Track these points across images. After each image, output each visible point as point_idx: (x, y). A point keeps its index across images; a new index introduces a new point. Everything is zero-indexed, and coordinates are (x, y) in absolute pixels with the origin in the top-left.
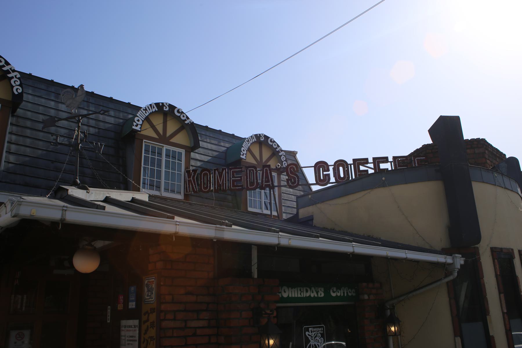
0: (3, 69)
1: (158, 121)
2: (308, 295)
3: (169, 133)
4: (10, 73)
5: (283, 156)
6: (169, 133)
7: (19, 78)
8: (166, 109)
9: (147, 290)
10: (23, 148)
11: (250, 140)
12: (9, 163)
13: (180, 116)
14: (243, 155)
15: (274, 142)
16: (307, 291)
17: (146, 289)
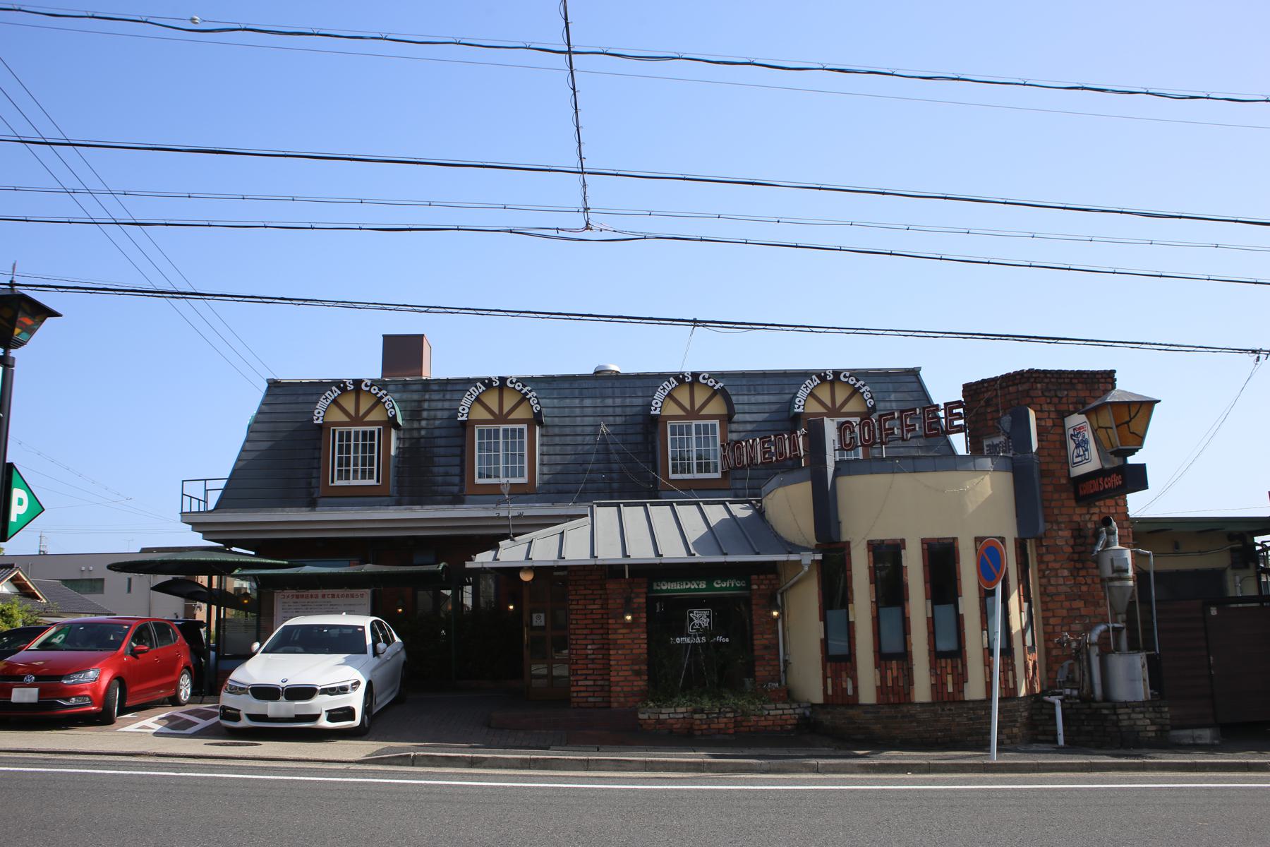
0: (856, 386)
2: (687, 587)
3: (839, 402)
6: (839, 402)
7: (869, 391)
9: (1075, 445)
10: (553, 457)
11: (473, 393)
12: (543, 474)
13: (848, 382)
16: (687, 584)
17: (1071, 445)
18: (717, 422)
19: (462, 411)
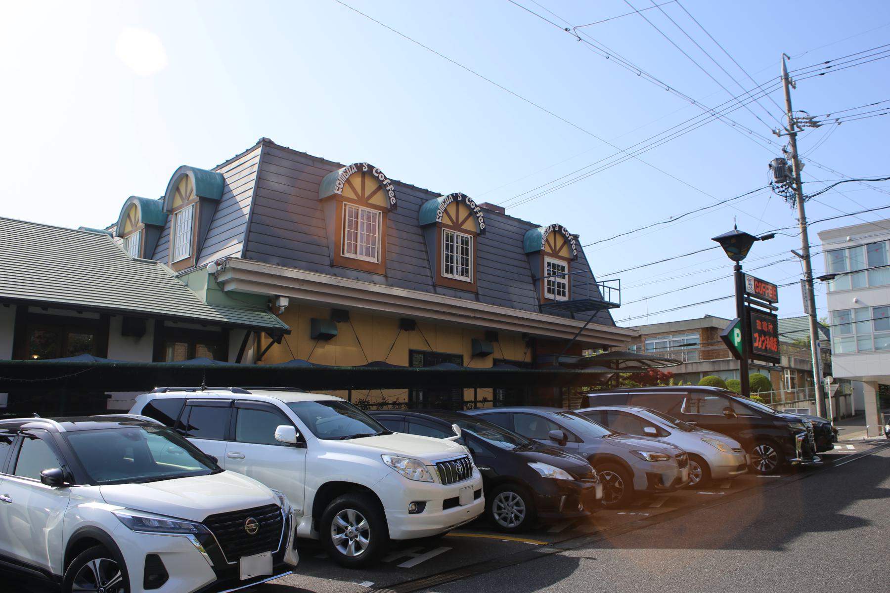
1: (357, 182)
4: (478, 213)
5: (391, 192)
7: (393, 191)
8: (365, 169)
11: (348, 171)
14: (439, 218)
15: (472, 201)
18: (377, 212)
19: (338, 185)
